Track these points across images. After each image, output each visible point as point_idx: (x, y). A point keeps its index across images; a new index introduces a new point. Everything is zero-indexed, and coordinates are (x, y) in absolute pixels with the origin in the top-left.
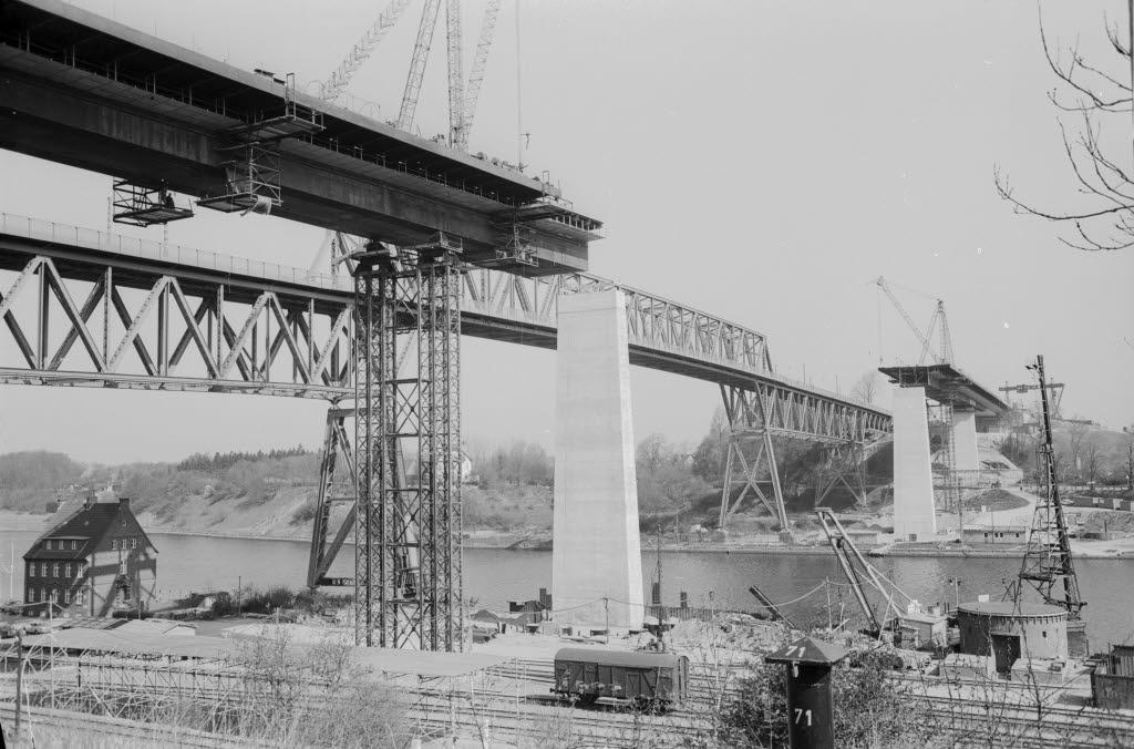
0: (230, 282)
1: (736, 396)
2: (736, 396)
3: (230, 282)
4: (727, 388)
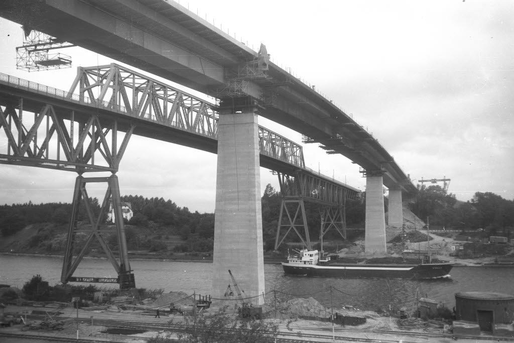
1: (285, 178)
2: (285, 178)
3: (316, 177)
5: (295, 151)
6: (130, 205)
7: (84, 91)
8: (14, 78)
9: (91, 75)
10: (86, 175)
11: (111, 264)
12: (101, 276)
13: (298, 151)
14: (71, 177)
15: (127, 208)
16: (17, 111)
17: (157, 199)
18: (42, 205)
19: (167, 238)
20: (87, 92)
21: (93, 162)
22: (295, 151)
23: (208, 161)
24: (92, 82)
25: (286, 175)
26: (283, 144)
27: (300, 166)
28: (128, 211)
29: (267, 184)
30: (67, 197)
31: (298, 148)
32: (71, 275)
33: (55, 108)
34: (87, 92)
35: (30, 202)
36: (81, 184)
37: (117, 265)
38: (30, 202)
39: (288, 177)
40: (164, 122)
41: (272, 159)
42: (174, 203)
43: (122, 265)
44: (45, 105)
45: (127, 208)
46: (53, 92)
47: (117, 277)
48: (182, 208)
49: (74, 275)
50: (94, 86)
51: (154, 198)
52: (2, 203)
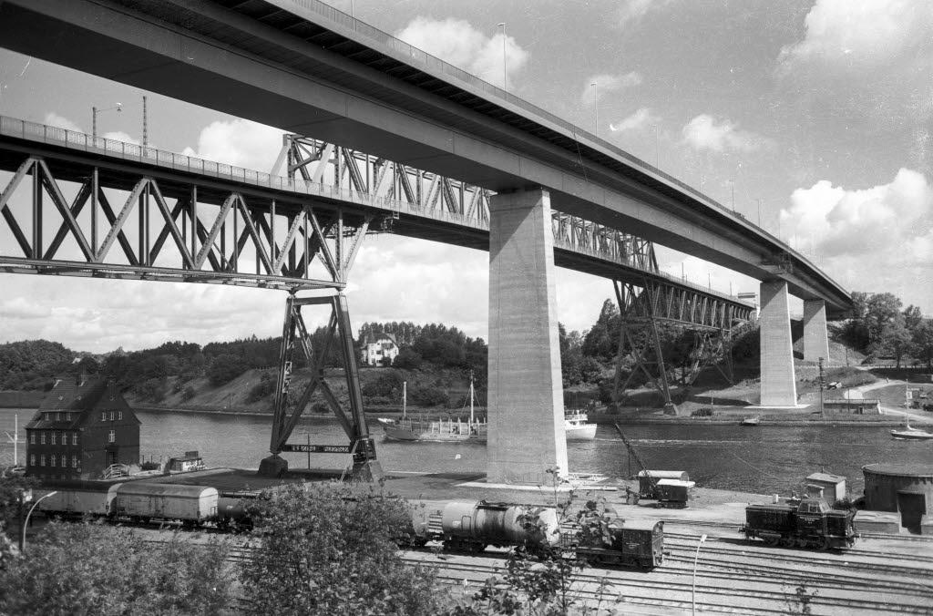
0: (204, 184)
1: (626, 290)
2: (626, 290)
3: (204, 184)
4: (619, 284)
5: (640, 246)
6: (393, 337)
7: (295, 170)
8: (211, 163)
9: (304, 146)
10: (300, 294)
11: (342, 429)
12: (325, 444)
13: (645, 247)
14: (276, 300)
15: (390, 342)
16: (267, 216)
17: (433, 326)
18: (270, 339)
19: (449, 385)
20: (298, 170)
21: (307, 275)
22: (640, 246)
23: (476, 263)
24: (305, 156)
25: (628, 285)
26: (619, 236)
27: (648, 269)
28: (391, 346)
29: (605, 300)
30: (270, 325)
31: (644, 242)
32: (285, 441)
33: (246, 197)
34: (298, 170)
35: (254, 336)
36: (294, 307)
37: (350, 427)
38: (254, 336)
39: (631, 289)
40: (595, 253)
41: (638, 272)
42: (461, 332)
43: (355, 426)
44: (230, 193)
45: (390, 342)
46: (214, 168)
47: (348, 445)
48: (475, 339)
49: (288, 443)
50: (309, 161)
51: (430, 325)
52: (3, 342)
